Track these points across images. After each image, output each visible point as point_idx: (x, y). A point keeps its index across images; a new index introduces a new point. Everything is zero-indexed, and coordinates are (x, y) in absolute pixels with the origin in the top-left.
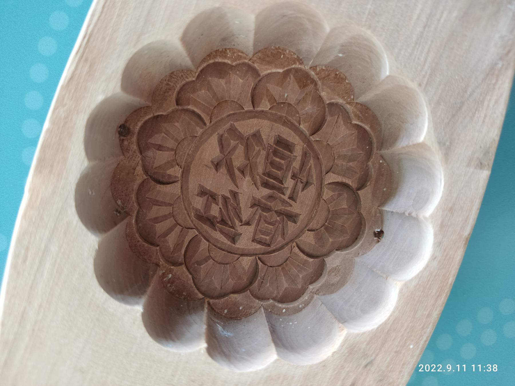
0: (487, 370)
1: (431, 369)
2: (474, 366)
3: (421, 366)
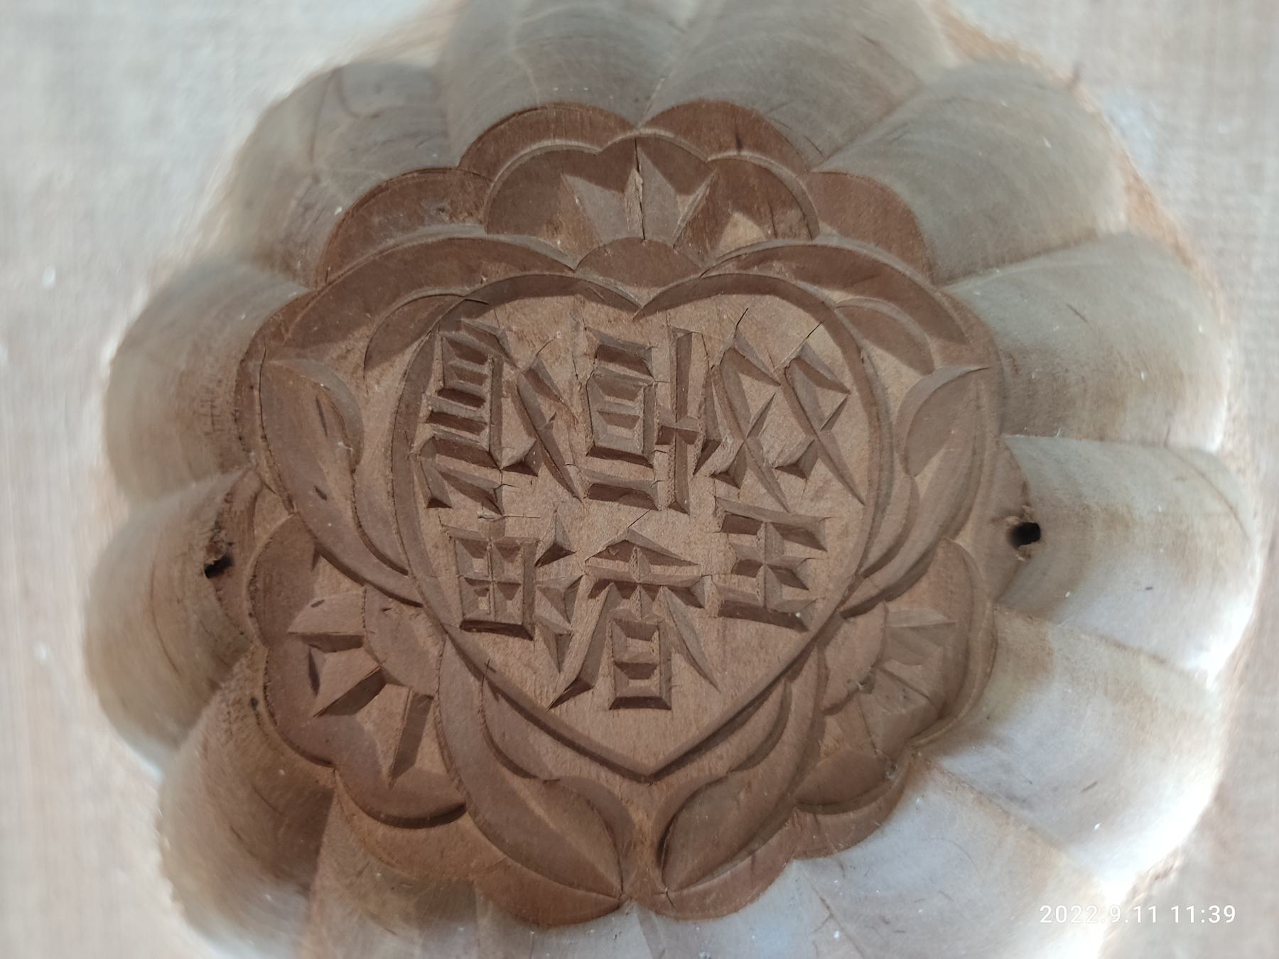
0: (1210, 920)
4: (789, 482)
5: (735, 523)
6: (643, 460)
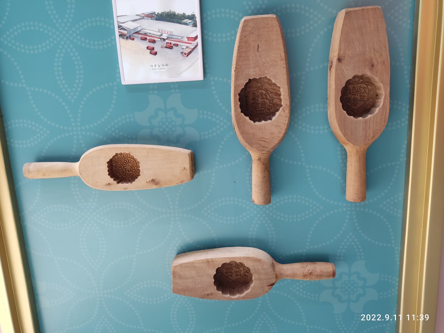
1: (371, 318)
2: (408, 315)
3: (363, 316)
4: (364, 94)
5: (360, 96)
6: (355, 93)
